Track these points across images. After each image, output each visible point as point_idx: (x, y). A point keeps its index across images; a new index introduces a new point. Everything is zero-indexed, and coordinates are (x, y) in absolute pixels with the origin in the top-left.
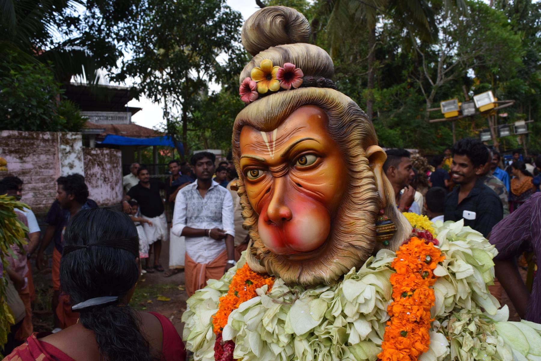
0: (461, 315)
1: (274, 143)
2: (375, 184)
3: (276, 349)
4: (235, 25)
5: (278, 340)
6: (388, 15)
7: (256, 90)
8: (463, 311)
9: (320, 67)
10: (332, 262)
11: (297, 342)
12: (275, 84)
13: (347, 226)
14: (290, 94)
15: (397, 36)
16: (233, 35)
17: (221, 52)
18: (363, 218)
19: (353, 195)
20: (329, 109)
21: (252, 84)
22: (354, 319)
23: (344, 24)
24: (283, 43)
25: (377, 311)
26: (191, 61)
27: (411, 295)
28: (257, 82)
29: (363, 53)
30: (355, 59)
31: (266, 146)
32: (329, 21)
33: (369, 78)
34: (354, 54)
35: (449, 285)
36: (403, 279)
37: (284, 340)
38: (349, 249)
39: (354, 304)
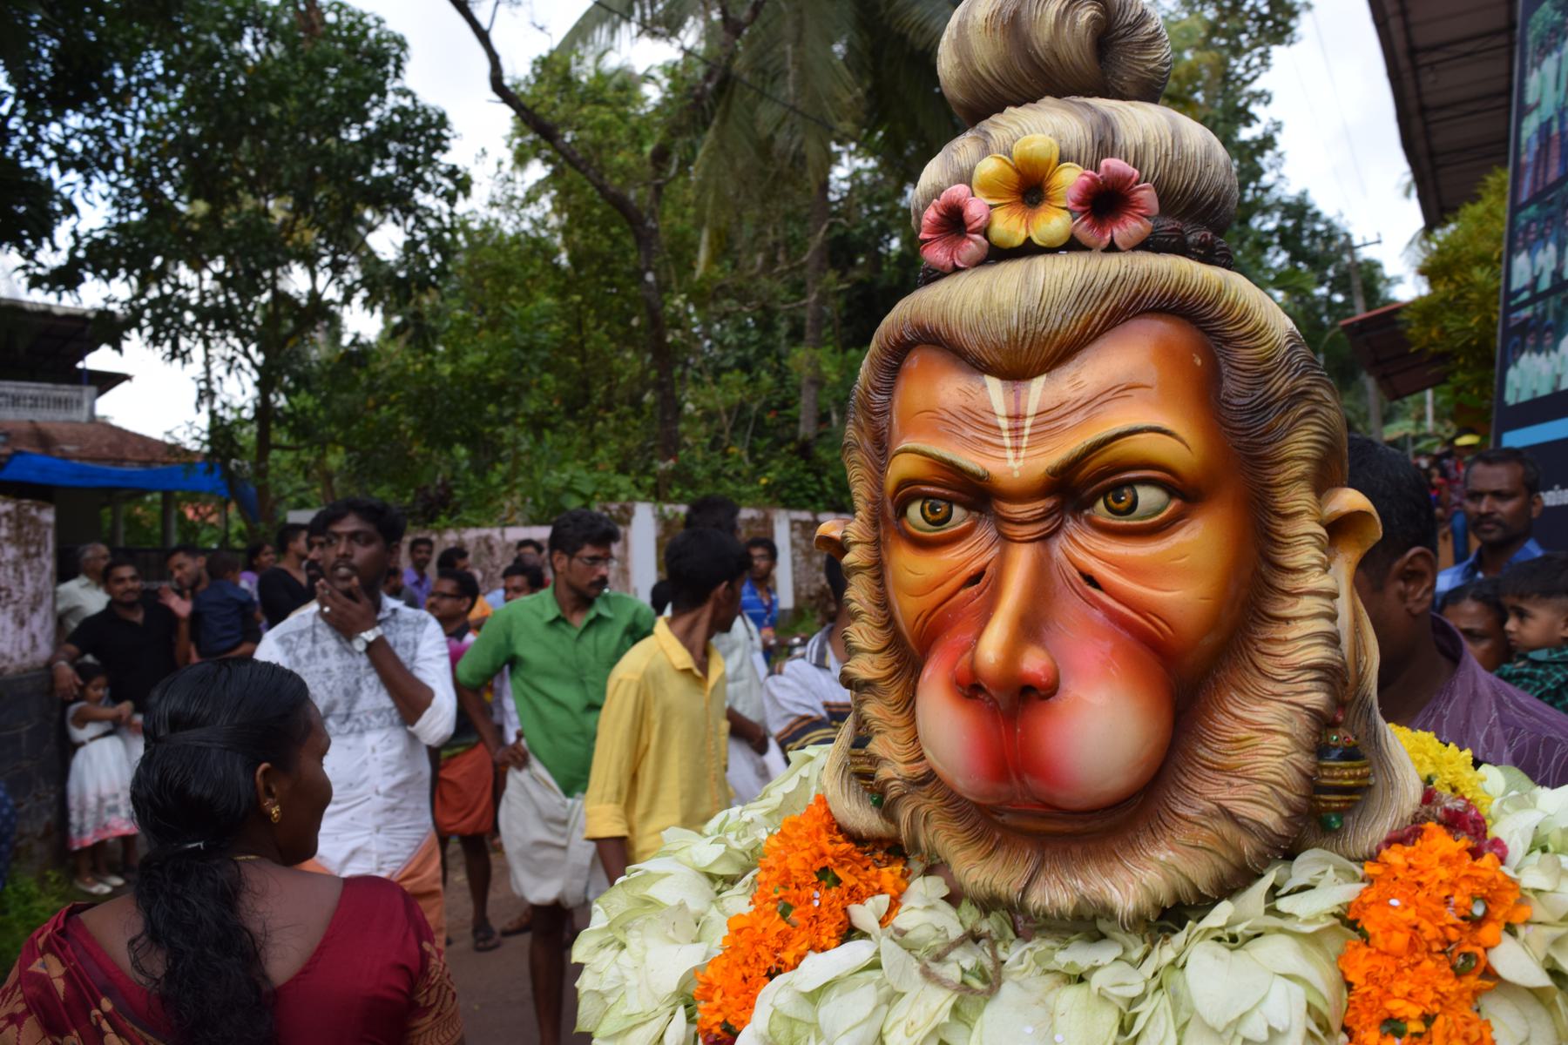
1: (1028, 422)
7: (985, 232)
15: (887, 206)
16: (421, 175)
17: (382, 222)
18: (1287, 729)
21: (976, 208)
23: (740, 164)
26: (289, 243)
27: (1419, 1035)
28: (992, 207)
29: (793, 245)
30: (771, 261)
31: (999, 428)
32: (700, 153)
33: (807, 315)
36: (1392, 971)
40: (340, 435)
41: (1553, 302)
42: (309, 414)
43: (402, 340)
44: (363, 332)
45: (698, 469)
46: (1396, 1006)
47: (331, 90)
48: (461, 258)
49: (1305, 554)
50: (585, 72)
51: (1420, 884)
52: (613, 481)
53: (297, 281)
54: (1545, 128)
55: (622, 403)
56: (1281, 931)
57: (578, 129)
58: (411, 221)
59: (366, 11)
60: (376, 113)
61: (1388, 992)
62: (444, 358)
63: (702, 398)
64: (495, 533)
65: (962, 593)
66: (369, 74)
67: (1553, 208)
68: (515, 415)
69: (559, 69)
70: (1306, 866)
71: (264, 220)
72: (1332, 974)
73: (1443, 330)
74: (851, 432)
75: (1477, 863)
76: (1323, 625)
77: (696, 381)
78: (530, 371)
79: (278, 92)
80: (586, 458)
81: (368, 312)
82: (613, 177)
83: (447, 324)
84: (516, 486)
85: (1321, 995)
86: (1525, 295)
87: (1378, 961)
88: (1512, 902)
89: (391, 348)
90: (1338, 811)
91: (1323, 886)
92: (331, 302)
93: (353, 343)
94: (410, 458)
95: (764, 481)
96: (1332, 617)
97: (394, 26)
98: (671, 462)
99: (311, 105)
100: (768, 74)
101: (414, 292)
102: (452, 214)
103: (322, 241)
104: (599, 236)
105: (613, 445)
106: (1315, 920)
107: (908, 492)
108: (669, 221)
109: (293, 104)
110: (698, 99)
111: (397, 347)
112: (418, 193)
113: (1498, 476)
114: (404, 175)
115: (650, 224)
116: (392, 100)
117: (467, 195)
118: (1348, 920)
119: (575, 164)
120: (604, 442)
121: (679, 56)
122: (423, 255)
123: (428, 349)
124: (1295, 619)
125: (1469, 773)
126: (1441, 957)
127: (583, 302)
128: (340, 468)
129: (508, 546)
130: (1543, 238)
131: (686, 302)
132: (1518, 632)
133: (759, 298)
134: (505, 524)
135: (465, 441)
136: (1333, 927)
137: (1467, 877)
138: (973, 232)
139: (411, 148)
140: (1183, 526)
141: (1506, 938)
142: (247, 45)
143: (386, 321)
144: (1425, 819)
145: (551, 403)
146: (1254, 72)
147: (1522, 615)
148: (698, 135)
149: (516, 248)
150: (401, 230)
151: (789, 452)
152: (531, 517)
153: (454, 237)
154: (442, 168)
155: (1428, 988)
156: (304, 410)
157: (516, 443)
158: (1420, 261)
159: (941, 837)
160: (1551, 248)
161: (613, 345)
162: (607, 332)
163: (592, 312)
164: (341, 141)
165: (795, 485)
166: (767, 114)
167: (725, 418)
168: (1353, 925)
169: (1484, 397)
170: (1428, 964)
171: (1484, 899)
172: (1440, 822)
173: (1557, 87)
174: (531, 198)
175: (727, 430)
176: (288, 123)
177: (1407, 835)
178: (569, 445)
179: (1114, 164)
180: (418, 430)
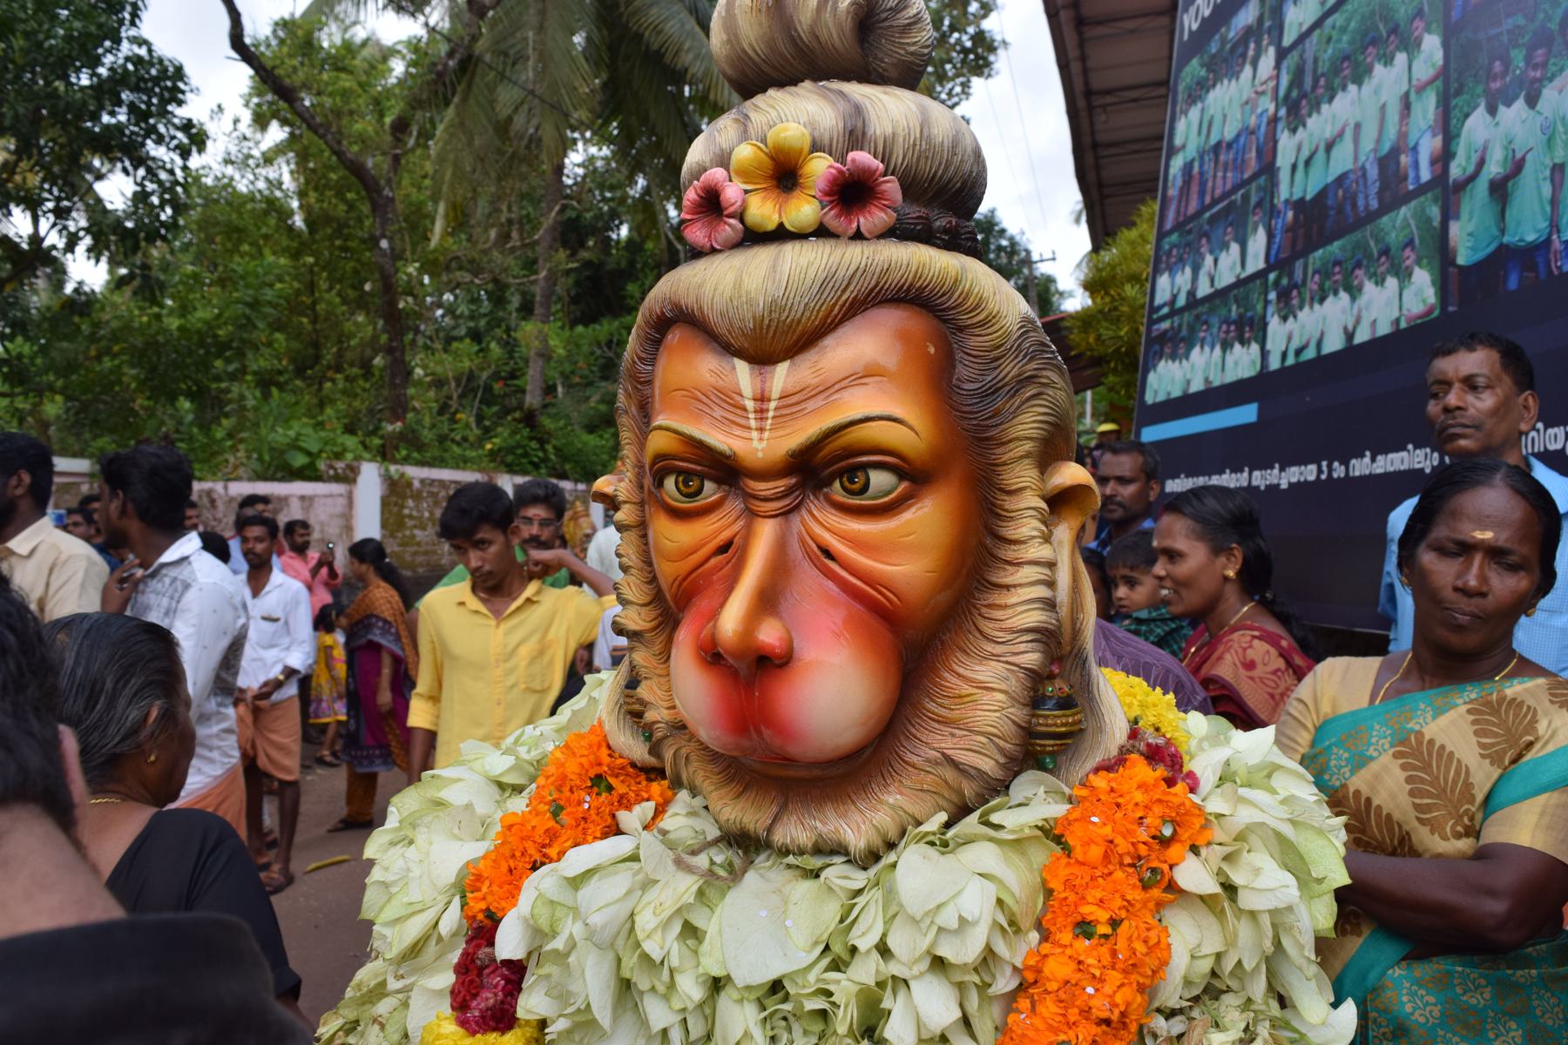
0: (1223, 1008)
1: (773, 405)
2: (1051, 584)
3: (659, 1015)
4: (161, 97)
5: (672, 985)
6: (602, 138)
7: (741, 217)
8: (1227, 999)
9: (950, 181)
10: (881, 802)
11: (725, 1001)
12: (804, 210)
13: (946, 702)
14: (853, 256)
15: (618, 194)
16: (154, 126)
17: (110, 171)
18: (1003, 686)
19: (984, 610)
20: (961, 329)
21: (732, 192)
22: (915, 971)
23: (477, 143)
24: (846, 77)
25: (989, 957)
26: (10, 185)
27: (1106, 936)
28: (746, 192)
29: (527, 223)
30: (505, 237)
31: (745, 410)
32: (440, 128)
33: (537, 290)
34: (502, 225)
35: (1209, 921)
36: (1088, 879)
37: (691, 989)
38: (940, 770)
39: (924, 926)
40: (60, 383)
41: (1187, 317)
42: (26, 361)
43: (127, 291)
44: (88, 281)
45: (425, 432)
47: (61, 32)
48: (194, 214)
50: (329, 38)
52: (340, 441)
54: (1188, 167)
55: (352, 365)
56: (991, 840)
57: (319, 94)
58: (141, 172)
60: (108, 59)
61: (1083, 898)
62: (172, 311)
64: (219, 487)
65: (713, 561)
66: (103, 19)
67: (1191, 237)
69: (300, 33)
75: (1172, 790)
76: (1042, 592)
77: (427, 348)
80: (313, 417)
81: (93, 261)
82: (350, 144)
83: (177, 278)
84: (241, 441)
86: (1165, 310)
87: (1076, 870)
88: (1198, 826)
89: (117, 298)
90: (1052, 754)
92: (54, 247)
93: (76, 290)
95: (489, 446)
98: (399, 424)
99: (39, 45)
100: (511, 58)
101: (143, 244)
102: (185, 168)
103: (46, 186)
104: (334, 201)
107: (661, 467)
108: (405, 191)
109: (19, 42)
110: (440, 75)
111: (123, 298)
115: (387, 192)
116: (126, 48)
117: (201, 149)
119: (313, 128)
120: (332, 402)
121: (422, 32)
122: (152, 206)
124: (1015, 586)
126: (1131, 870)
127: (316, 264)
128: (58, 417)
129: (231, 500)
130: (1181, 261)
135: (190, 395)
137: (1159, 801)
138: (730, 216)
139: (145, 98)
140: (910, 506)
143: (111, 272)
145: (280, 360)
146: (955, 99)
147: (1132, 583)
150: (131, 179)
154: (176, 121)
155: (1117, 896)
156: (20, 356)
158: (1082, 277)
160: (1188, 270)
161: (344, 308)
162: (339, 295)
163: (325, 275)
165: (519, 451)
166: (506, 96)
167: (453, 384)
168: (1058, 840)
169: (1130, 397)
170: (1119, 875)
173: (1199, 133)
174: (268, 159)
175: (455, 396)
176: (13, 62)
178: (297, 403)
179: (862, 157)
180: (142, 383)
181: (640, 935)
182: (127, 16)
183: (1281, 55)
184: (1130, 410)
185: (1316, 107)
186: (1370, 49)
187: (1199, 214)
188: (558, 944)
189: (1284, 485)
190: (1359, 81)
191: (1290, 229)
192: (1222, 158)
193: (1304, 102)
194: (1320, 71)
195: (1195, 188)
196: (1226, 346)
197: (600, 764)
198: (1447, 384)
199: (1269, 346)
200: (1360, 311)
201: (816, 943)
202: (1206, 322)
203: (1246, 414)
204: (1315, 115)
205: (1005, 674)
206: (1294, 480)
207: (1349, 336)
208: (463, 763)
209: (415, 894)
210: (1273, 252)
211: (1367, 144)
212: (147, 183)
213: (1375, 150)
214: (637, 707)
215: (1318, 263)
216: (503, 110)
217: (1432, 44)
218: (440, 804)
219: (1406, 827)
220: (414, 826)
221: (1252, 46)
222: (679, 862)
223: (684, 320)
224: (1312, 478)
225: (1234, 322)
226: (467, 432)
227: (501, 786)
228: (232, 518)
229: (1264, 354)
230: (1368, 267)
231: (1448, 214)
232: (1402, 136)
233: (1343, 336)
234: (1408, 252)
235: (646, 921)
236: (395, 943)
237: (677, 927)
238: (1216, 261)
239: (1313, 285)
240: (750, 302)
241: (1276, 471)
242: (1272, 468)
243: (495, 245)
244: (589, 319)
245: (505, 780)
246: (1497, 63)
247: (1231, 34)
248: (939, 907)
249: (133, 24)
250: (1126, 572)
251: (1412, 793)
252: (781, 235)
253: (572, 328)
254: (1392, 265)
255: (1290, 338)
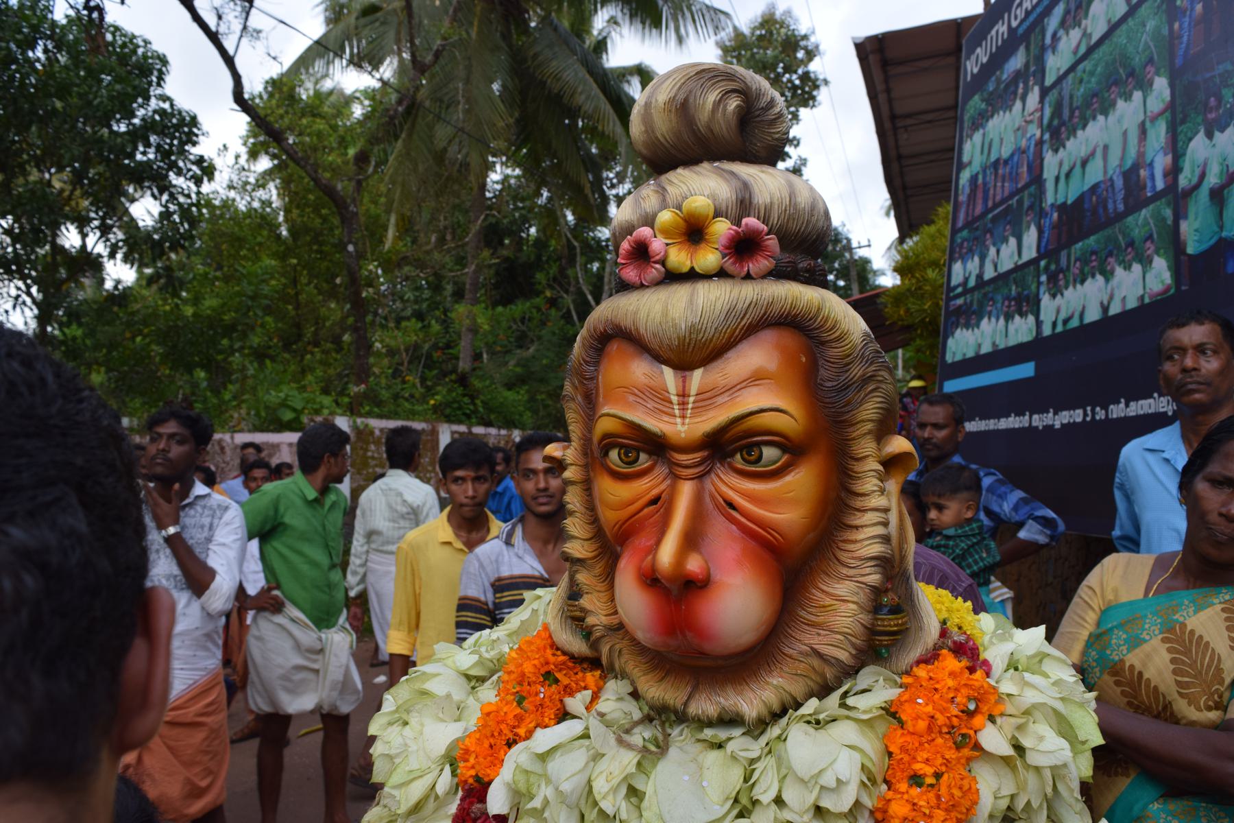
1: (691, 399)
4: (180, 139)
6: (513, 160)
7: (663, 262)
16: (175, 162)
17: (142, 197)
18: (855, 599)
21: (657, 245)
23: (421, 168)
24: (732, 158)
26: (67, 208)
27: (932, 786)
28: (667, 245)
30: (442, 240)
32: (391, 159)
35: (1005, 771)
36: (917, 745)
41: (977, 295)
42: (79, 341)
43: (155, 287)
45: (383, 392)
46: (919, 767)
49: (870, 484)
51: (936, 690)
52: (318, 400)
53: (70, 238)
54: (974, 179)
56: (848, 718)
58: (165, 197)
59: (136, 33)
60: (141, 113)
61: (914, 758)
63: (387, 340)
65: (646, 510)
66: (137, 82)
67: (978, 233)
68: (242, 348)
70: (866, 677)
71: (47, 190)
72: (879, 746)
73: (907, 311)
74: (568, 388)
78: (255, 314)
79: (63, 91)
80: (298, 382)
83: (191, 276)
84: (243, 401)
85: (871, 759)
86: (960, 290)
87: (909, 739)
89: (145, 292)
90: (887, 646)
91: (876, 691)
94: (159, 378)
95: (432, 402)
96: (885, 524)
97: (158, 46)
99: (90, 103)
100: (445, 103)
102: (198, 193)
105: (319, 373)
106: (870, 711)
108: (366, 207)
110: (392, 118)
112: (172, 175)
113: (937, 413)
114: (162, 161)
115: (352, 208)
116: (154, 103)
117: (211, 179)
118: (890, 712)
120: (312, 370)
121: (378, 85)
123: (176, 295)
125: (971, 617)
127: (298, 264)
128: (102, 384)
129: (236, 447)
130: (971, 251)
131: (376, 267)
132: (938, 519)
133: (433, 267)
134: (234, 430)
135: (203, 367)
136: (880, 716)
137: (965, 685)
138: (656, 262)
141: (989, 724)
142: (39, 53)
144: (941, 648)
145: (271, 339)
147: (940, 508)
148: (390, 143)
149: (248, 221)
150: (158, 203)
151: (451, 381)
152: (254, 425)
153: (199, 210)
154: (191, 157)
156: (74, 338)
157: (244, 368)
159: (628, 662)
160: (976, 259)
161: (321, 298)
162: (316, 287)
164: (111, 132)
165: (455, 405)
168: (894, 715)
170: (940, 741)
171: (977, 700)
172: (950, 650)
173: (982, 152)
174: (261, 184)
177: (929, 658)
178: (285, 371)
179: (751, 221)
181: (598, 797)
182: (154, 79)
183: (1044, 93)
184: (933, 367)
185: (1073, 132)
186: (1113, 88)
187: (984, 214)
188: (537, 803)
189: (1058, 426)
190: (1105, 113)
191: (1056, 227)
192: (1000, 171)
193: (1063, 129)
194: (1075, 105)
195: (980, 195)
196: (1009, 317)
197: (547, 663)
198: (1182, 350)
199: (1042, 317)
200: (1112, 290)
201: (727, 799)
202: (992, 299)
203: (1026, 370)
204: (1072, 139)
205: (856, 590)
206: (1065, 421)
207: (1105, 309)
208: (439, 660)
209: (414, 763)
210: (1043, 244)
211: (1114, 161)
212: (170, 205)
213: (1120, 166)
214: (578, 614)
215: (1079, 253)
216: (440, 142)
217: (1161, 85)
218: (425, 693)
219: (1169, 698)
220: (408, 712)
221: (1021, 85)
222: (620, 741)
223: (621, 336)
224: (1079, 420)
225: (1014, 299)
226: (414, 391)
227: (468, 677)
228: (237, 461)
229: (1039, 324)
230: (1117, 256)
231: (1179, 215)
232: (1141, 154)
233: (1100, 309)
234: (1148, 244)
235: (600, 786)
236: (403, 801)
237: (624, 791)
238: (998, 251)
239: (1075, 270)
240: (674, 326)
241: (1051, 415)
242: (1048, 412)
243: (436, 247)
244: (506, 301)
245: (473, 672)
246: (1212, 99)
247: (1005, 76)
248: (820, 772)
249: (159, 85)
250: (936, 500)
251: (1175, 672)
252: (692, 276)
253: (493, 308)
254: (1137, 254)
255: (1058, 311)
